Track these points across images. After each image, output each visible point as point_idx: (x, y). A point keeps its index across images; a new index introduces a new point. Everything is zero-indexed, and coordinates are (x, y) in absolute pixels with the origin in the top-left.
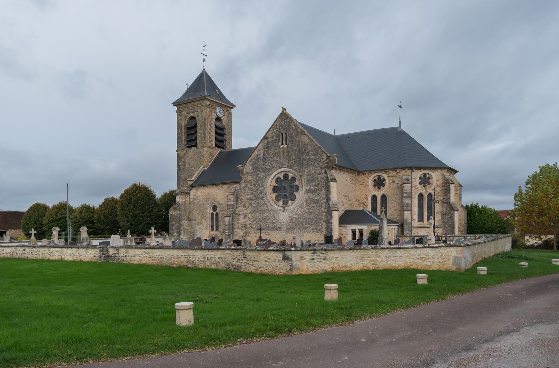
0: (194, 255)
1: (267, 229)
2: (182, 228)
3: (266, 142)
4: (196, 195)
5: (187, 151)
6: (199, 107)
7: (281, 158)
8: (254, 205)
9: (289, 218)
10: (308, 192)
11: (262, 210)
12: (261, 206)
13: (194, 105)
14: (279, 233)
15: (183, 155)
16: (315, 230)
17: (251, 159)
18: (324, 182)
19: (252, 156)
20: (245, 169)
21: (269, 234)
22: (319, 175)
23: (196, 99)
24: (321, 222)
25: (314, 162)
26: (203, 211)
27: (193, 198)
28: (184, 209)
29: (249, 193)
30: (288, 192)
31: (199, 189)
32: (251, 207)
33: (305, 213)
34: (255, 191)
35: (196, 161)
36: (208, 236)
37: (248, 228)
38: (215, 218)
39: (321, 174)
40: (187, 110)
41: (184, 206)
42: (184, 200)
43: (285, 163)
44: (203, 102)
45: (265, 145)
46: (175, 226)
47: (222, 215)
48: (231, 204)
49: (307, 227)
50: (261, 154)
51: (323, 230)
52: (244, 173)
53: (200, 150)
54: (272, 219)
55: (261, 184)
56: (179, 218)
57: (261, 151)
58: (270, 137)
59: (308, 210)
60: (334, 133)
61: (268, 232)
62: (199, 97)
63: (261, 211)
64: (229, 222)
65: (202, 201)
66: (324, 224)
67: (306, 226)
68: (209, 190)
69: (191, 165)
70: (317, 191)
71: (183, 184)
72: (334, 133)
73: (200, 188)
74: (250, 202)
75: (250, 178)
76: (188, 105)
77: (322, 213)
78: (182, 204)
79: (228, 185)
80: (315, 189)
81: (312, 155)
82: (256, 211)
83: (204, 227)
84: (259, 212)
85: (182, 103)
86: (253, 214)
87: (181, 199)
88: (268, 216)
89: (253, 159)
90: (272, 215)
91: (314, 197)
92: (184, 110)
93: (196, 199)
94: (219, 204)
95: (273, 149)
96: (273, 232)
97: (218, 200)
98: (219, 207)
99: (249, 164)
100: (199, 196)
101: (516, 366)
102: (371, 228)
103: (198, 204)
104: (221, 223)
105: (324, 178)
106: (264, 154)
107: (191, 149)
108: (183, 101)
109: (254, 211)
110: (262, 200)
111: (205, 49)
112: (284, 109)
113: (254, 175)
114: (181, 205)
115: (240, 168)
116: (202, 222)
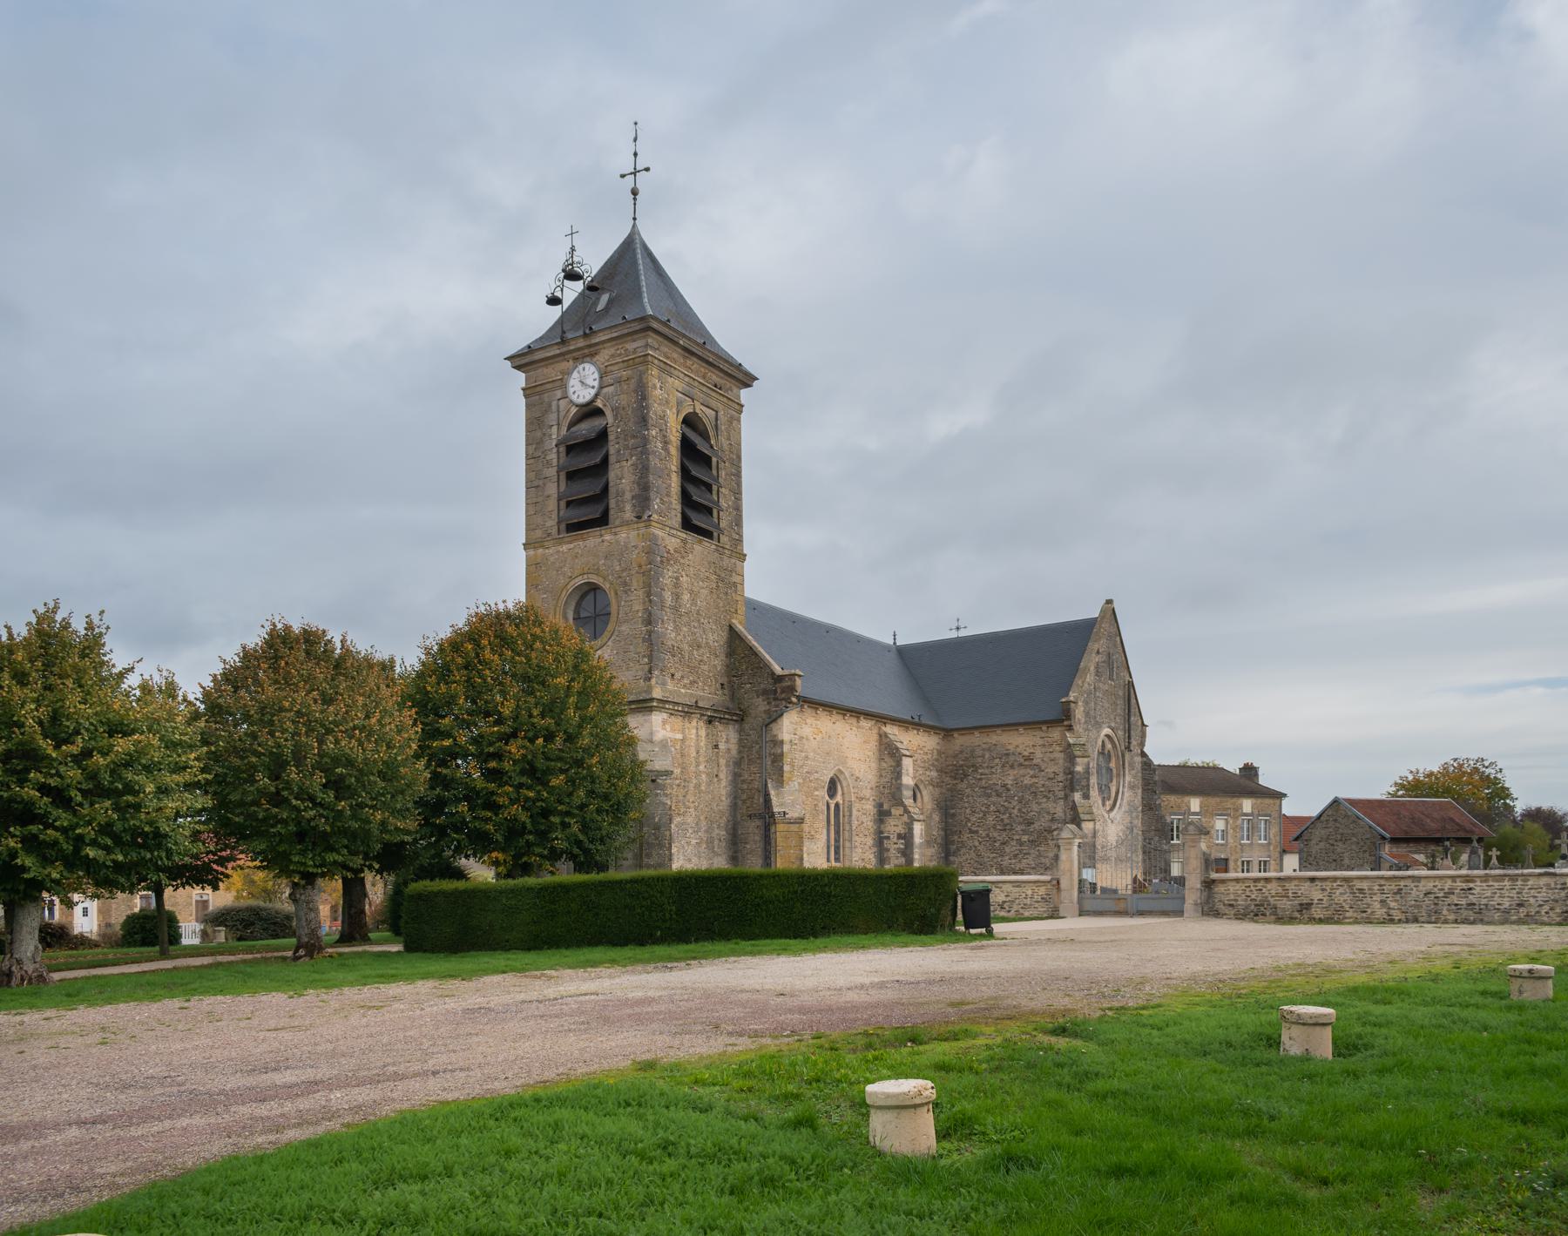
0: (896, 978)
5: (684, 541)
6: (721, 398)
15: (672, 552)
26: (816, 793)
27: (791, 741)
35: (715, 596)
41: (681, 761)
42: (680, 736)
62: (695, 342)
76: (689, 363)
85: (681, 342)
87: (668, 727)
92: (676, 373)
101: (1385, 1232)
107: (700, 542)
108: (690, 339)
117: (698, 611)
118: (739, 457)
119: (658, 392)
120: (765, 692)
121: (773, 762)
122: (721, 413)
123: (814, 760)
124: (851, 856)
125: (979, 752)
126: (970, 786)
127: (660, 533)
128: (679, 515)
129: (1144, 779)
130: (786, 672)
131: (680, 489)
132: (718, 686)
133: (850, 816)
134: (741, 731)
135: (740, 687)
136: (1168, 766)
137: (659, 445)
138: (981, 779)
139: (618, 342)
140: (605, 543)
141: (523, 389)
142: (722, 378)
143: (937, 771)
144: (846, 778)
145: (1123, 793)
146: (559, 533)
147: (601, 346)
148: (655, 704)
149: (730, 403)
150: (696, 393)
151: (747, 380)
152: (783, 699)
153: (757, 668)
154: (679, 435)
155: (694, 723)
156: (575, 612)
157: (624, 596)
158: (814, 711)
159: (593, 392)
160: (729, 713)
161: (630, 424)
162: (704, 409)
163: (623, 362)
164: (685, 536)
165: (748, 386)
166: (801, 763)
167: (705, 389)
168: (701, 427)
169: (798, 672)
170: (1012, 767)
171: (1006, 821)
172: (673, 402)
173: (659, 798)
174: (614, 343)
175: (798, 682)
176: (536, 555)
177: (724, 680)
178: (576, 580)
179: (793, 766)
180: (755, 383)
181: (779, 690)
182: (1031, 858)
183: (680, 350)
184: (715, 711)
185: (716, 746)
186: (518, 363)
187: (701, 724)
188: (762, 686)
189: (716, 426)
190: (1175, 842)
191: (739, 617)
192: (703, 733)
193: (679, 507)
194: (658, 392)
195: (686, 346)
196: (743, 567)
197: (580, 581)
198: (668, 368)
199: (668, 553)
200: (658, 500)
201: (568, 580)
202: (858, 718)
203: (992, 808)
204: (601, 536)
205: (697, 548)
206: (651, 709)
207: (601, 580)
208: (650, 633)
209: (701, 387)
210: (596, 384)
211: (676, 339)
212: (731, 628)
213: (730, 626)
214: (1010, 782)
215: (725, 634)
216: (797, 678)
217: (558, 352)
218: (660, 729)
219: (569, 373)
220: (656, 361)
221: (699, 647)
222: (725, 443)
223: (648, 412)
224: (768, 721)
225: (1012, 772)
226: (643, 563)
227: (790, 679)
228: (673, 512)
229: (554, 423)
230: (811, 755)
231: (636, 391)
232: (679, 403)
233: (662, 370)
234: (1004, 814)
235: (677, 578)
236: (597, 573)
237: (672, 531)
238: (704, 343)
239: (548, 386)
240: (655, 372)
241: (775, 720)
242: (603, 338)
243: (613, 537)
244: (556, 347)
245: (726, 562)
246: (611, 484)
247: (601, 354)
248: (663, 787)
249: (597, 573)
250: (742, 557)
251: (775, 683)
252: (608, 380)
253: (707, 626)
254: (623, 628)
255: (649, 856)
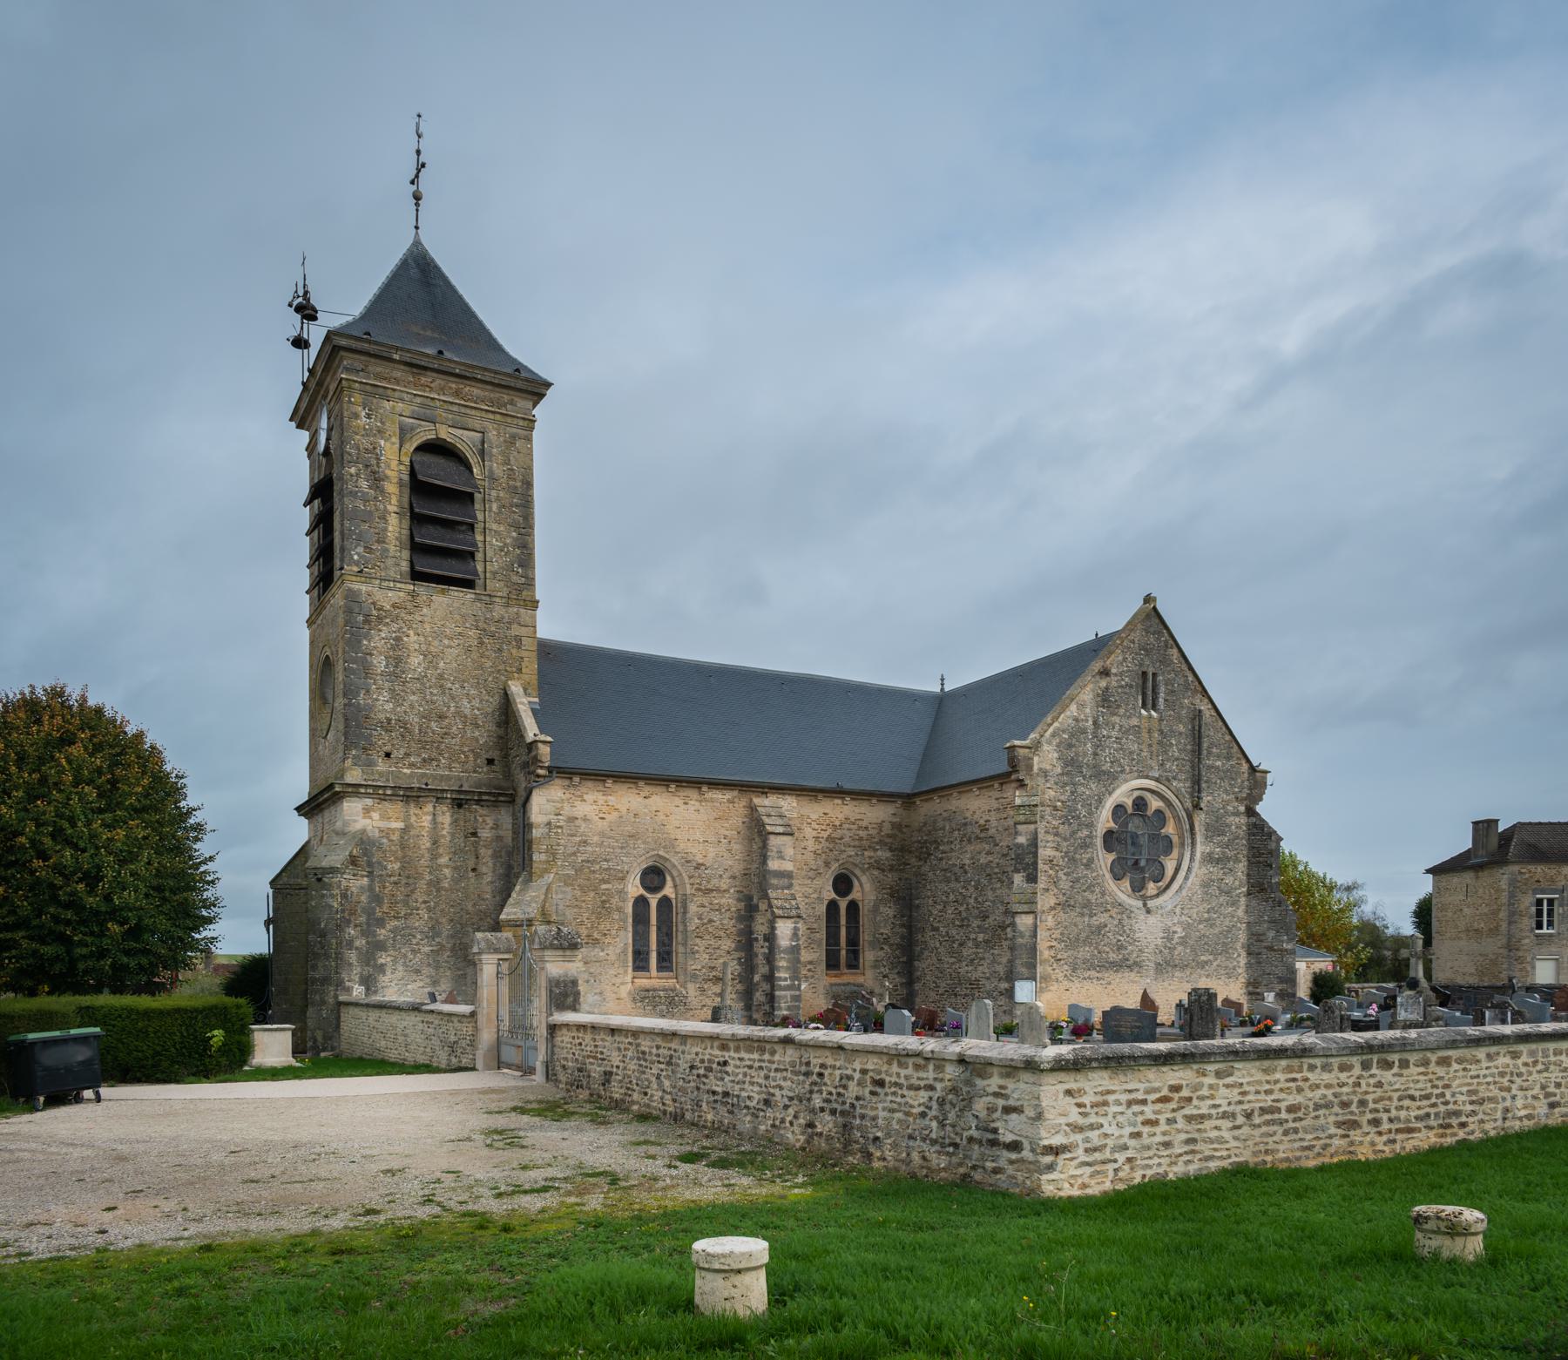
1: (1103, 966)
2: (381, 961)
3: (1103, 684)
4: (567, 810)
5: (413, 594)
7: (1144, 747)
8: (1065, 884)
9: (1162, 935)
10: (1209, 859)
11: (1087, 904)
12: (1085, 891)
13: (457, 393)
14: (1137, 979)
16: (1223, 972)
17: (1058, 729)
18: (1242, 839)
19: (1060, 720)
20: (1036, 759)
21: (1109, 983)
22: (1232, 818)
23: (488, 377)
24: (1236, 949)
25: (1222, 779)
26: (604, 886)
27: (549, 823)
28: (397, 866)
29: (1048, 842)
30: (1143, 852)
31: (584, 790)
32: (1056, 891)
33: (1200, 922)
34: (1065, 839)
35: (475, 655)
36: (630, 993)
37: (1046, 961)
38: (843, 921)
39: (1237, 814)
40: (419, 400)
42: (401, 825)
43: (1154, 764)
44: (512, 403)
45: (1098, 695)
46: (357, 949)
47: (701, 910)
48: (782, 869)
49: (1206, 962)
50: (1087, 721)
51: (1240, 971)
52: (1036, 768)
54: (1118, 933)
55: (1084, 816)
56: (370, 913)
57: (1088, 711)
58: (1116, 675)
59: (1208, 912)
60: (942, 684)
61: (1106, 975)
63: (1085, 906)
64: (792, 940)
65: (601, 845)
66: (1244, 954)
67: (1203, 958)
68: (640, 799)
69: (442, 664)
70: (1228, 859)
71: (387, 749)
72: (942, 684)
73: (590, 784)
74: (1051, 872)
75: (1052, 793)
77: (1239, 925)
79: (735, 793)
80: (1223, 853)
81: (1218, 757)
82: (1069, 906)
83: (613, 958)
84: (1078, 910)
85: (396, 357)
86: (1061, 914)
87: (375, 815)
88: (1106, 926)
89: (1064, 731)
90: (1116, 922)
91: (1220, 875)
94: (688, 862)
95: (1122, 711)
96: (1120, 975)
97: (682, 846)
98: (690, 877)
99: (1049, 743)
102: (1312, 966)
103: (574, 854)
104: (698, 941)
105: (1245, 828)
106: (1095, 723)
109: (1065, 905)
110: (1088, 872)
112: (1148, 599)
113: (1066, 784)
114: (380, 848)
115: (1022, 752)
116: (596, 935)
122: (492, 435)
124: (686, 964)
125: (940, 824)
126: (933, 869)
129: (1251, 848)
133: (685, 913)
136: (1559, 823)
137: (364, 484)
138: (941, 859)
143: (891, 850)
144: (674, 866)
145: (1189, 869)
162: (459, 432)
170: (969, 841)
171: (964, 915)
173: (325, 900)
179: (554, 855)
180: (549, 392)
182: (986, 964)
190: (1545, 931)
202: (700, 788)
203: (952, 897)
211: (385, 354)
214: (967, 862)
216: (540, 745)
225: (970, 848)
234: (962, 905)
248: (329, 887)
255: (314, 967)
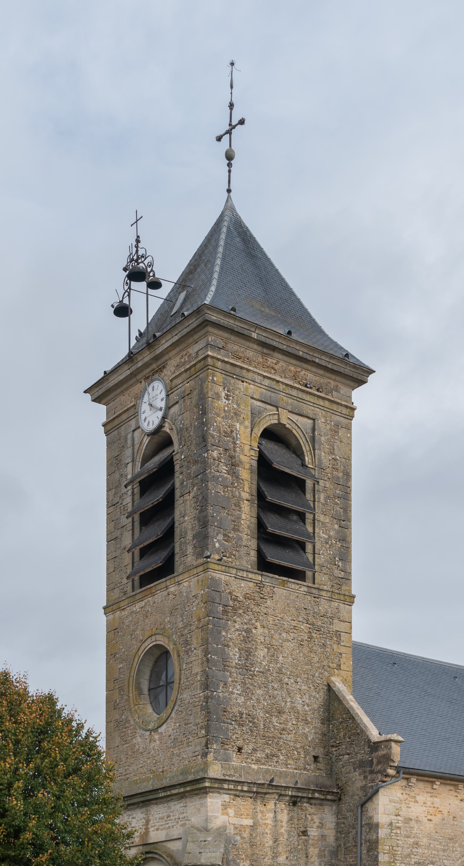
5: (260, 585)
6: (321, 402)
15: (241, 598)
27: (391, 824)
35: (306, 650)
42: (249, 822)
53: (324, 606)
65: (428, 847)
76: (271, 361)
78: (238, 838)
85: (254, 335)
87: (231, 812)
92: (250, 375)
93: (404, 833)
100: (417, 821)
103: (409, 856)
107: (283, 584)
108: (265, 330)
111: (234, 101)
117: (280, 669)
118: (348, 475)
119: (223, 402)
120: (361, 764)
121: (369, 850)
122: (320, 422)
123: (428, 847)
127: (223, 577)
128: (253, 554)
130: (383, 738)
131: (254, 521)
132: (310, 759)
134: (338, 813)
135: (338, 760)
137: (224, 468)
139: (181, 347)
140: (171, 596)
141: (104, 425)
142: (322, 376)
146: (133, 590)
147: (166, 357)
148: (207, 784)
149: (335, 407)
150: (283, 399)
151: (372, 372)
152: (379, 772)
153: (354, 734)
154: (255, 455)
155: (271, 805)
156: (150, 681)
157: (185, 657)
158: (429, 785)
159: (160, 414)
160: (320, 792)
161: (193, 448)
162: (295, 418)
163: (186, 371)
164: (260, 578)
165: (361, 382)
166: (407, 851)
167: (294, 393)
168: (294, 442)
169: (395, 737)
172: (246, 412)
174: (177, 349)
175: (396, 749)
176: (114, 619)
177: (320, 752)
178: (146, 644)
180: (371, 378)
181: (375, 761)
183: (255, 347)
184: (299, 789)
185: (305, 833)
186: (97, 395)
187: (282, 805)
188: (359, 757)
189: (313, 439)
191: (343, 673)
192: (284, 817)
193: (253, 544)
194: (223, 402)
195: (263, 339)
196: (350, 612)
197: (149, 644)
198: (238, 370)
199: (234, 600)
200: (220, 537)
201: (139, 644)
204: (167, 587)
205: (280, 591)
206: (204, 792)
207: (166, 640)
208: (207, 698)
209: (289, 391)
210: (162, 404)
211: (246, 332)
212: (330, 689)
213: (329, 686)
215: (320, 696)
216: (393, 744)
217: (128, 372)
218: (219, 814)
219: (139, 397)
220: (219, 364)
221: (280, 712)
222: (326, 459)
223: (208, 429)
224: (364, 799)
226: (201, 616)
227: (386, 747)
228: (243, 550)
229: (129, 460)
230: (424, 841)
231: (197, 406)
232: (255, 415)
233: (227, 373)
235: (248, 631)
236: (163, 632)
237: (240, 574)
238: (289, 333)
239: (124, 417)
240: (219, 377)
241: (370, 799)
242: (166, 346)
243: (176, 587)
244: (126, 367)
245: (324, 606)
246: (177, 524)
247: (168, 367)
249: (163, 632)
250: (349, 600)
251: (371, 752)
252: (174, 397)
253: (293, 687)
254: (185, 696)
